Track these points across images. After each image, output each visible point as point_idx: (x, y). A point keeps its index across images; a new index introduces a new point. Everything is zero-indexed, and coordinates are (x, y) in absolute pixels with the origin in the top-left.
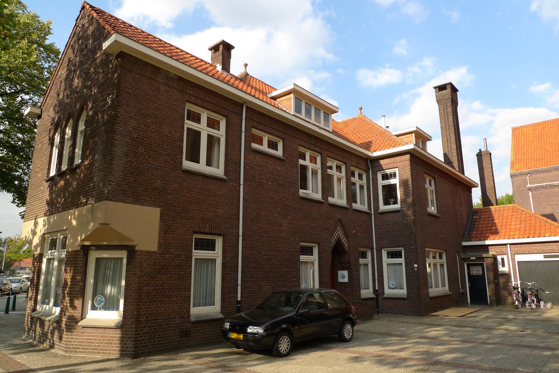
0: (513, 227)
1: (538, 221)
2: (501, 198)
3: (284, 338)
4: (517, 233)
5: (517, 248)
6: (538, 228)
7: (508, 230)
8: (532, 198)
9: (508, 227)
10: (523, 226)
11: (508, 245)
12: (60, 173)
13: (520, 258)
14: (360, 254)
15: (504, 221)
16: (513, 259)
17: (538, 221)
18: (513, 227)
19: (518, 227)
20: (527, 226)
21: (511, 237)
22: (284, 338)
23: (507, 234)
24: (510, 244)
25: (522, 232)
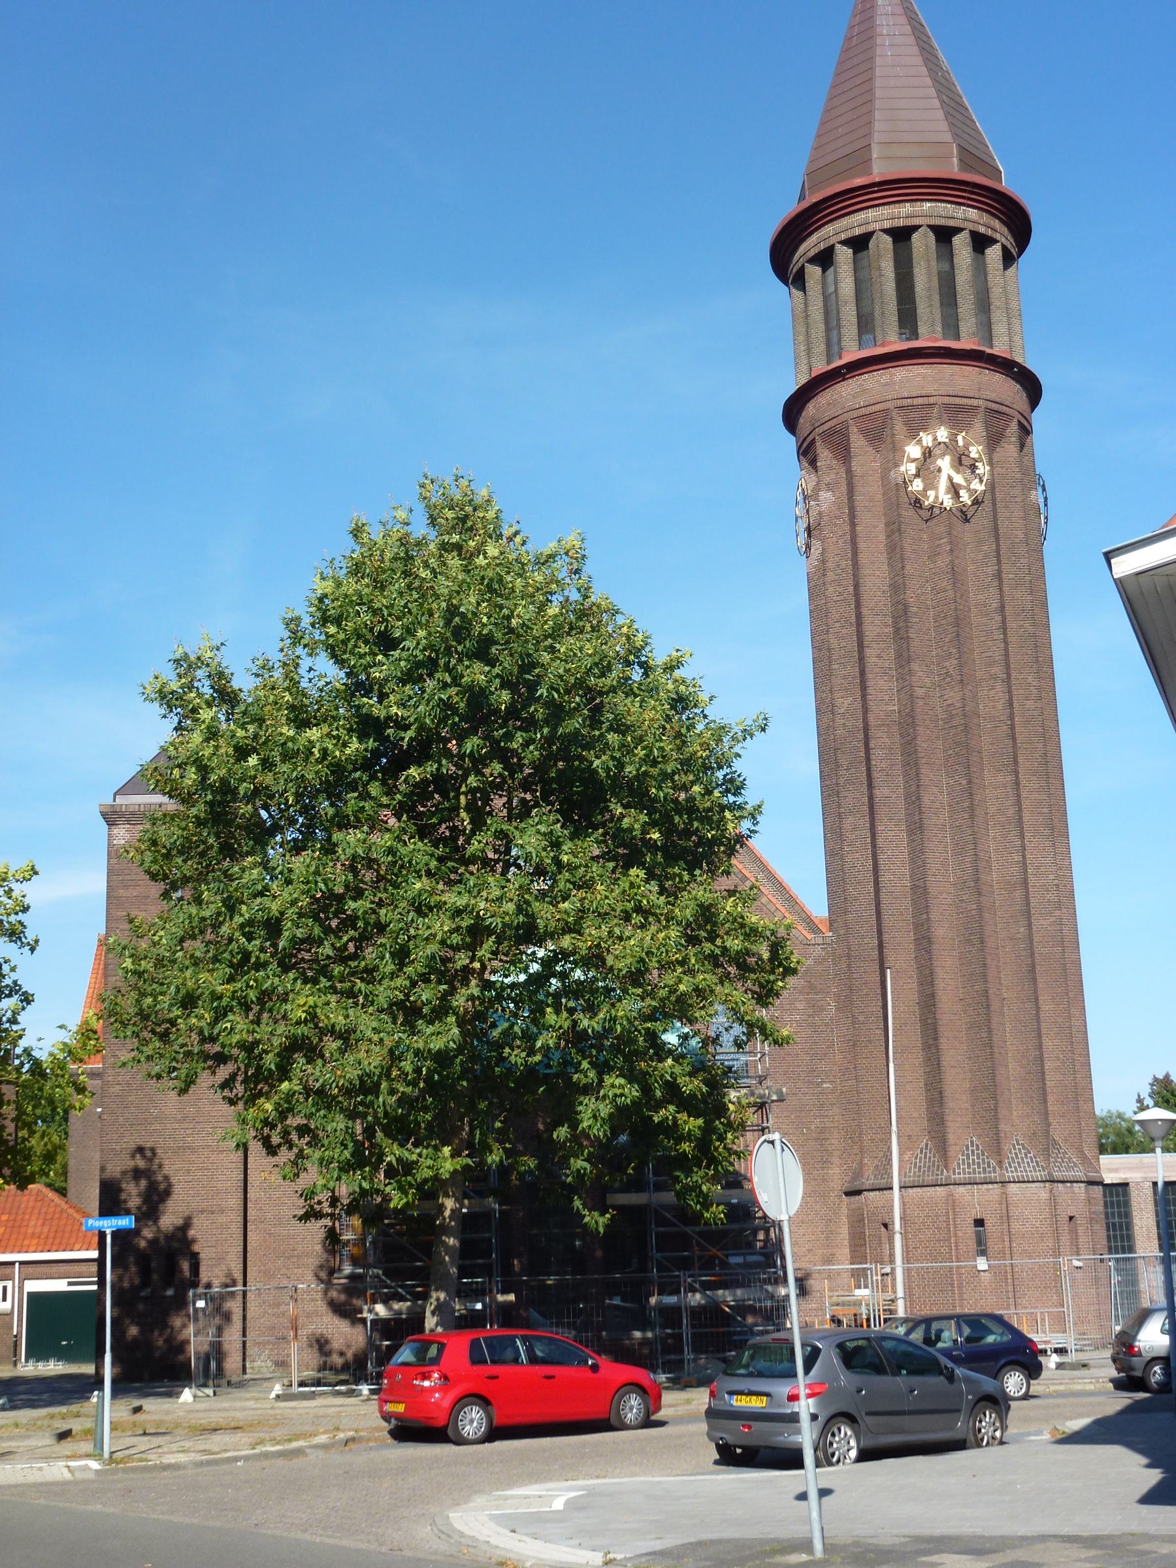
0: (30, 1231)
1: (70, 1222)
2: (1104, 1114)
3: (836, 1431)
4: (35, 1241)
5: (30, 1269)
6: (67, 1235)
7: (21, 1237)
8: (899, 1137)
9: (23, 1230)
10: (46, 1229)
11: (17, 1264)
12: (906, 1338)
13: (33, 1286)
14: (1058, 1239)
15: (20, 1217)
16: (21, 1288)
17: (70, 1222)
18: (30, 1231)
19: (38, 1230)
20: (54, 1229)
21: (24, 1249)
22: (836, 1431)
23: (19, 1242)
24: (22, 1263)
25: (42, 1241)
